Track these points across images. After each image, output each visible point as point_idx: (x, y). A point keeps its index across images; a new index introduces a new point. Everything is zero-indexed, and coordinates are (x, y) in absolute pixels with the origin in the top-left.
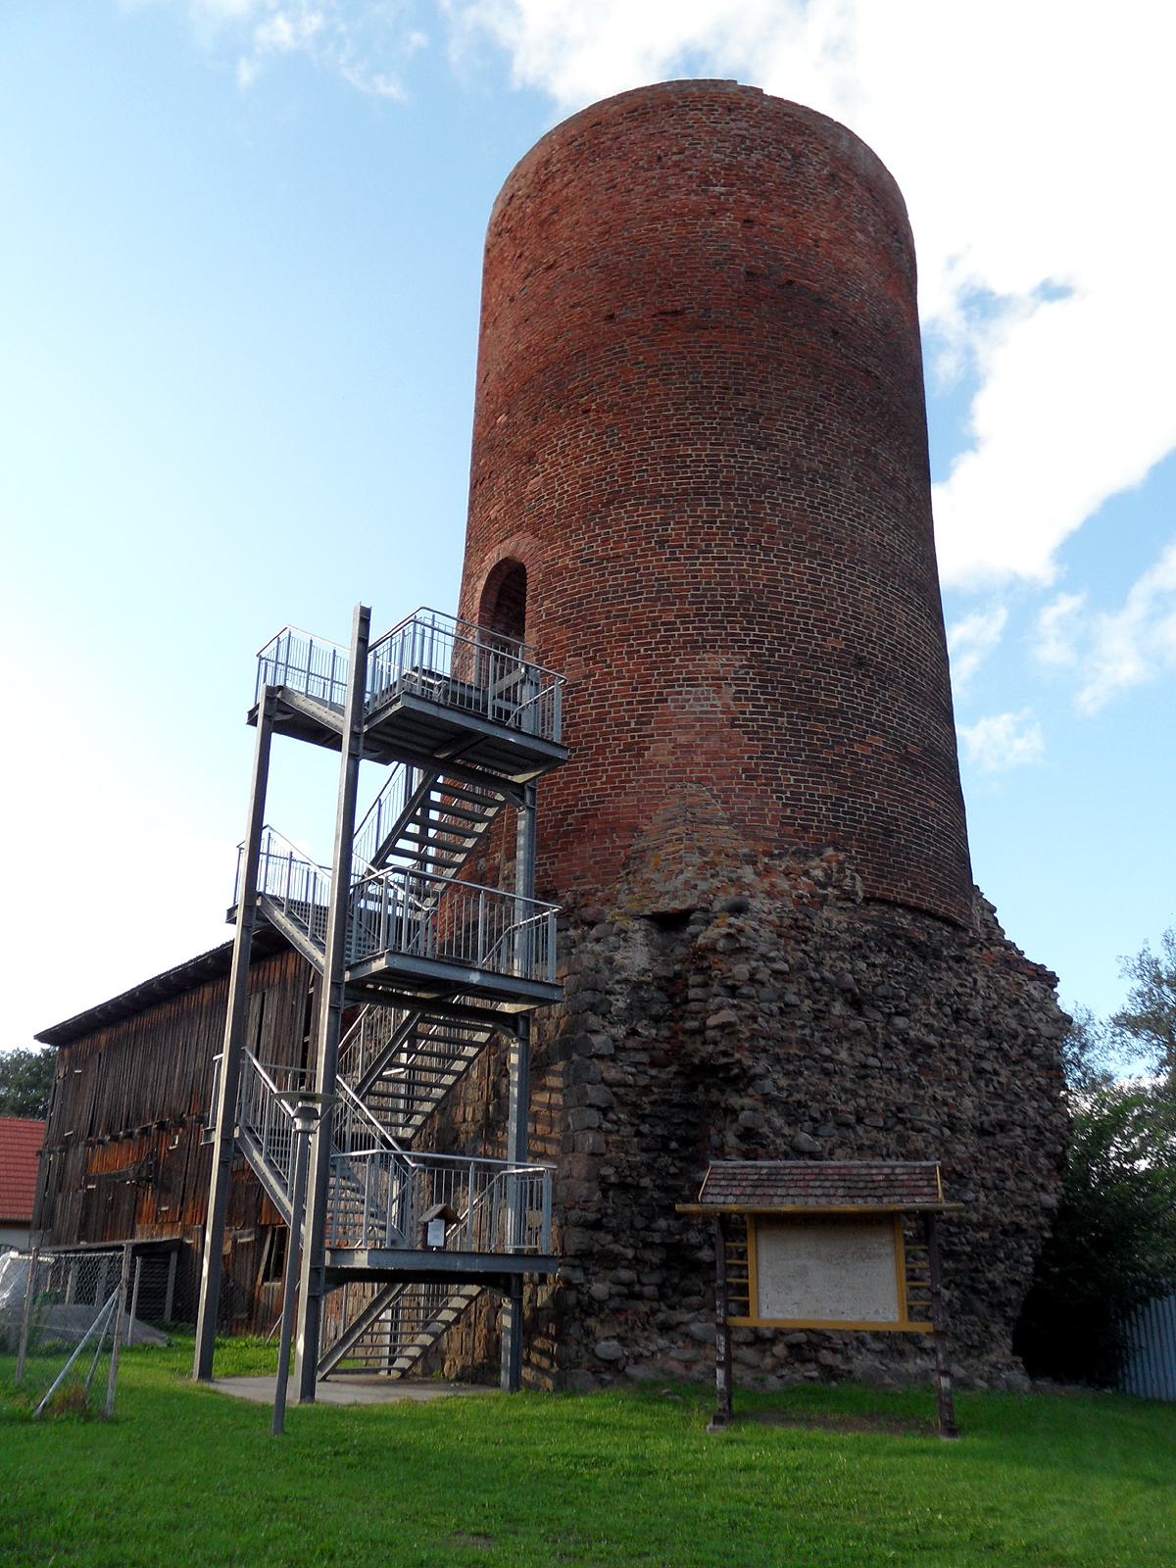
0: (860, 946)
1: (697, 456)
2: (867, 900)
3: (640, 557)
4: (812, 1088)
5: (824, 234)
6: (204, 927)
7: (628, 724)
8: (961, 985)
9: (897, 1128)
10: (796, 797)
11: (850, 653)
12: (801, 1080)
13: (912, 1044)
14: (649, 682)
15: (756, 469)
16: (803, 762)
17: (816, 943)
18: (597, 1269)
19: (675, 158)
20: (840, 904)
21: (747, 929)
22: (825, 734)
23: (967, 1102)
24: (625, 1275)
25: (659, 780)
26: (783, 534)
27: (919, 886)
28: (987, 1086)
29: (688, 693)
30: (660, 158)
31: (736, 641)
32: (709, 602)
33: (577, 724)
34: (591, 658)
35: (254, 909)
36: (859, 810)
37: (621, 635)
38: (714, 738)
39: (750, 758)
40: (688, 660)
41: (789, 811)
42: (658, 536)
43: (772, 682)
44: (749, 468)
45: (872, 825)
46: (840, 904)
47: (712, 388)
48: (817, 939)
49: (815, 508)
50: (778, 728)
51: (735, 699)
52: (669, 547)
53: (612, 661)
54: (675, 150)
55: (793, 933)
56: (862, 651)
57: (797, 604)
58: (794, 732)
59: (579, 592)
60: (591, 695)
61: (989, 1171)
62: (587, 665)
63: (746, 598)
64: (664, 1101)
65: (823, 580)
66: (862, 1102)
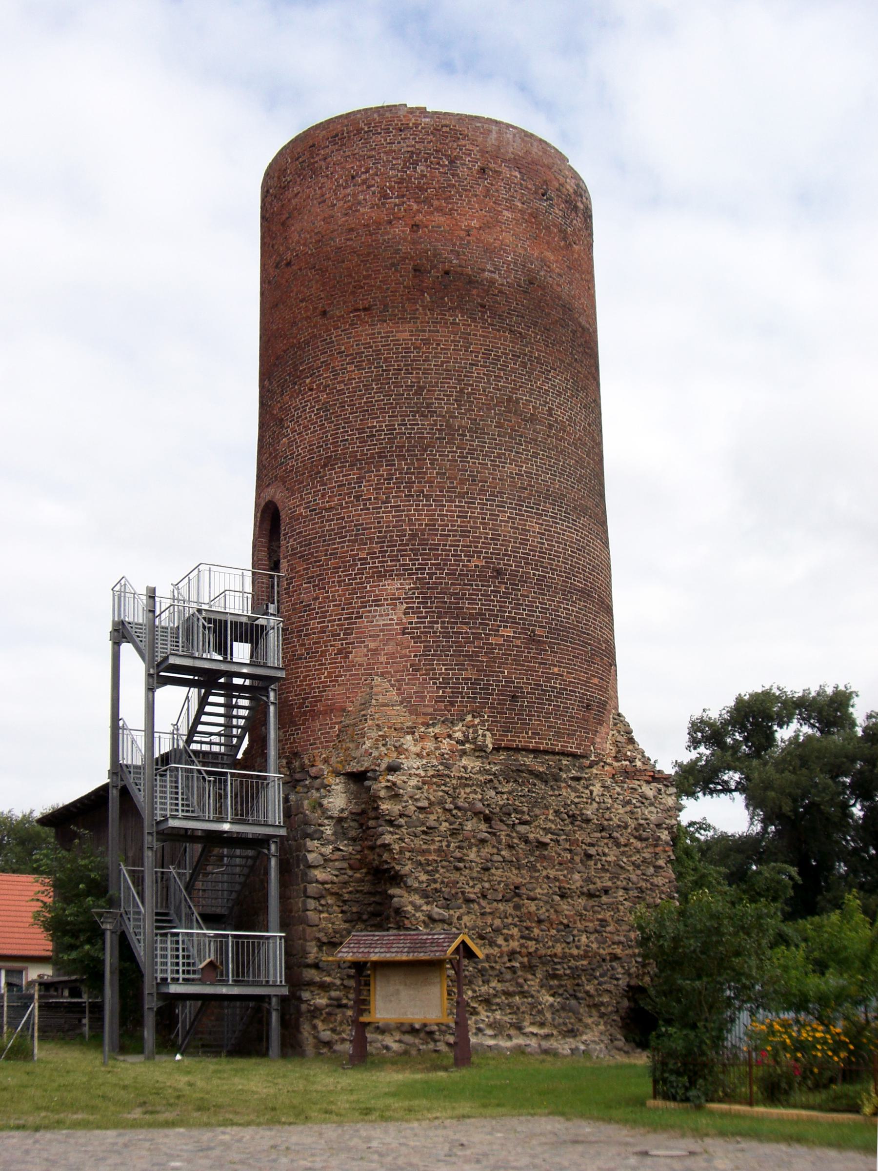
0: (491, 781)
1: (380, 426)
2: (497, 749)
3: (345, 508)
4: (446, 880)
5: (474, 223)
6: (96, 776)
7: (339, 635)
8: (578, 797)
9: (515, 900)
10: (446, 681)
11: (489, 568)
12: (437, 876)
13: (530, 843)
14: (351, 603)
15: (420, 433)
16: (451, 655)
17: (453, 784)
18: (319, 992)
19: (364, 177)
20: (477, 754)
21: (398, 782)
22: (468, 633)
23: (577, 876)
24: (333, 994)
25: (358, 675)
26: (440, 482)
27: (538, 734)
28: (595, 865)
29: (376, 611)
30: (353, 177)
31: (407, 570)
32: (388, 542)
33: (310, 634)
34: (317, 585)
35: (117, 769)
36: (492, 685)
37: (334, 568)
38: (392, 643)
39: (415, 656)
40: (375, 586)
41: (441, 691)
42: (356, 492)
43: (430, 598)
44: (415, 433)
45: (502, 695)
46: (477, 754)
47: (390, 370)
48: (454, 782)
49: (464, 457)
50: (435, 632)
51: (405, 614)
52: (363, 500)
53: (329, 588)
54: (363, 170)
55: (435, 780)
56: (499, 564)
57: (449, 536)
58: (446, 635)
59: (309, 535)
60: (317, 613)
61: (592, 921)
62: (315, 591)
63: (413, 536)
64: (357, 891)
65: (469, 514)
66: (487, 885)
